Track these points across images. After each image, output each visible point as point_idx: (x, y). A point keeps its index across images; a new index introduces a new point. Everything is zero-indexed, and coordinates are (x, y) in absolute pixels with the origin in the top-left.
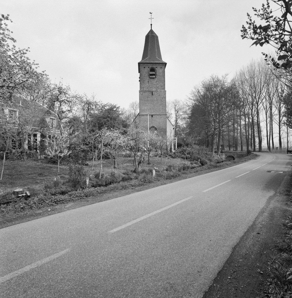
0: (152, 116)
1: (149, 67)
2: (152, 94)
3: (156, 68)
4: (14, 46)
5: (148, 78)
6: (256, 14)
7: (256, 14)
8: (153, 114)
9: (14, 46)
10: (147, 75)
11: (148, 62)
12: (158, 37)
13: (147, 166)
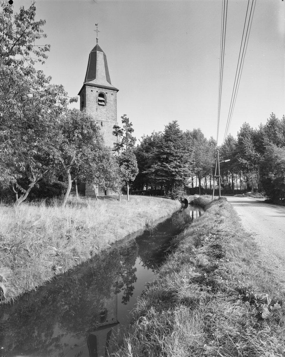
1: (97, 92)
2: (102, 124)
3: (106, 94)
5: (96, 105)
10: (95, 100)
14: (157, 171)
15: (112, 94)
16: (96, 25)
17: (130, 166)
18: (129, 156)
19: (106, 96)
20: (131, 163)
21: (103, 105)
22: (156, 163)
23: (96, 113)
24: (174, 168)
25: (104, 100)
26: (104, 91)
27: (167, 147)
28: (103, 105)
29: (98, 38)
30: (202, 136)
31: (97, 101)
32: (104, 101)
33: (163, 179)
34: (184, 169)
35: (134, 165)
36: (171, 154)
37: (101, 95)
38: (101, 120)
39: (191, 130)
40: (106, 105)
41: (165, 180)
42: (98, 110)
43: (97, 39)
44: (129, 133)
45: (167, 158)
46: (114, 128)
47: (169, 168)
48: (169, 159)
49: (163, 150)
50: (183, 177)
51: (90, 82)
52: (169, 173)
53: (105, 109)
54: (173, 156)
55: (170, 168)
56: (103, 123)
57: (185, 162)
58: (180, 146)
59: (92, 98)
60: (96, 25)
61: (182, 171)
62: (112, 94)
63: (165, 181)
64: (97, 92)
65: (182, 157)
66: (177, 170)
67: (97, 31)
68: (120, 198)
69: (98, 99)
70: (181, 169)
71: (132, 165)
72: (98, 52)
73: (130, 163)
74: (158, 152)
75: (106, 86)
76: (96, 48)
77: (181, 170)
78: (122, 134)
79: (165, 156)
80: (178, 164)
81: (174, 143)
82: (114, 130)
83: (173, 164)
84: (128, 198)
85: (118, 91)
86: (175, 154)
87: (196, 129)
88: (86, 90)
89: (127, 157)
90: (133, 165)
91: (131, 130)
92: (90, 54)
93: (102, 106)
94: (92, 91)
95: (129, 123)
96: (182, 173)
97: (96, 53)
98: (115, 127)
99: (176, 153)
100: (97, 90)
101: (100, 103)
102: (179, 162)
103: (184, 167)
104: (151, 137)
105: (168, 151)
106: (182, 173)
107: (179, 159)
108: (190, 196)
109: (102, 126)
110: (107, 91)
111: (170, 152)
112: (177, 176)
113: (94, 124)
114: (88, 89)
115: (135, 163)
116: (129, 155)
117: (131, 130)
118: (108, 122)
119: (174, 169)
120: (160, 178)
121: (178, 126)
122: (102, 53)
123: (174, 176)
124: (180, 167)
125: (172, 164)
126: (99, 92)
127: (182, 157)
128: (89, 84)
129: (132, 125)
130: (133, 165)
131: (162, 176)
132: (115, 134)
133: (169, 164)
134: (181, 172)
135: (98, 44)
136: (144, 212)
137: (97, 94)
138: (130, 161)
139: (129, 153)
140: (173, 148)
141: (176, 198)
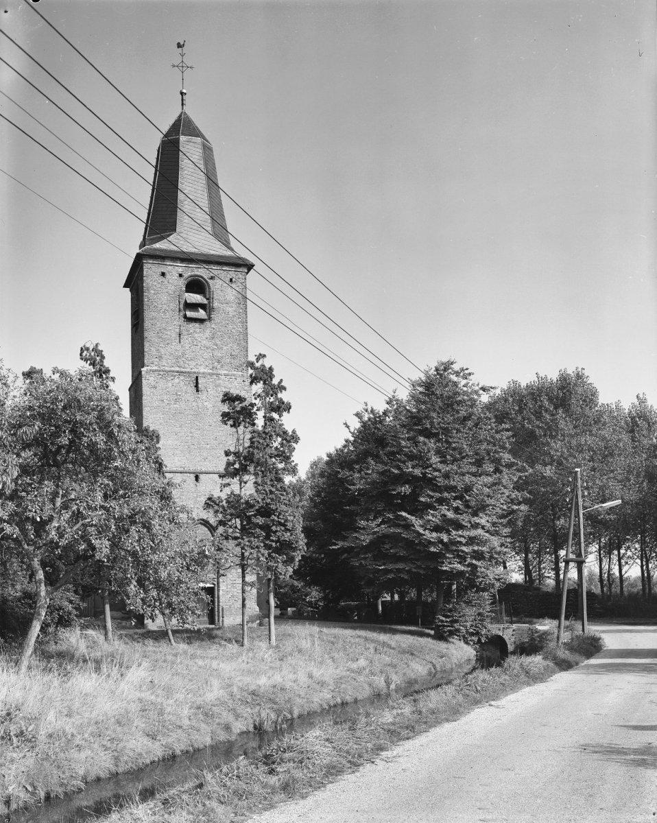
0: (197, 478)
1: (181, 275)
2: (197, 386)
3: (210, 282)
4: (54, 374)
5: (178, 321)
6: (467, 369)
7: (467, 369)
8: (199, 469)
9: (54, 374)
10: (174, 305)
11: (34, 6)
12: (212, 151)
13: (501, 427)
14: (379, 540)
15: (231, 280)
16: (179, 46)
17: (274, 528)
18: (273, 496)
19: (210, 288)
20: (276, 518)
21: (201, 321)
22: (378, 514)
23: (179, 347)
24: (437, 529)
25: (205, 301)
26: (202, 272)
27: (411, 457)
28: (201, 321)
29: (184, 91)
30: (590, 397)
31: (182, 306)
32: (203, 306)
33: (399, 571)
34: (473, 533)
35: (289, 525)
36: (430, 483)
37: (196, 285)
38: (196, 370)
39: (553, 376)
40: (210, 319)
41: (409, 572)
42: (184, 337)
43: (182, 93)
44: (275, 416)
45: (414, 496)
46: (223, 401)
47: (418, 533)
48: (422, 499)
49: (399, 468)
50: (469, 560)
51: (157, 245)
52: (417, 548)
53: (208, 333)
54: (437, 488)
55: (421, 531)
56: (200, 381)
57: (479, 509)
58: (461, 451)
59: (165, 298)
60: (179, 46)
61: (464, 541)
62: (231, 280)
63: (406, 577)
64: (181, 275)
65: (468, 489)
66: (445, 538)
67: (182, 67)
68: (246, 637)
69: (182, 302)
70: (460, 533)
71: (280, 524)
72: (182, 138)
73: (273, 520)
74: (382, 473)
75: (212, 252)
76: (183, 126)
77: (460, 536)
78: (254, 420)
79: (406, 489)
80: (450, 515)
81: (439, 440)
82: (226, 408)
83: (433, 517)
84: (273, 638)
85: (250, 267)
86: (441, 482)
87: (571, 371)
88: (145, 273)
89: (263, 499)
90: (284, 525)
91: (282, 407)
92: (159, 148)
93: (197, 325)
94: (163, 274)
95: (275, 381)
96: (464, 548)
97: (177, 142)
98: (228, 398)
99: (447, 476)
100: (180, 270)
101: (190, 314)
102: (457, 510)
103: (476, 526)
104: (385, 413)
105: (418, 472)
106: (464, 548)
107: (455, 498)
108: (514, 626)
109: (197, 391)
110: (216, 270)
111: (424, 474)
112: (447, 558)
113: (108, 417)
114: (151, 270)
115: (290, 518)
116: (271, 492)
117: (282, 407)
118: (218, 375)
119: (434, 535)
120: (390, 567)
121: (470, 374)
122: (199, 140)
123: (438, 557)
124: (459, 526)
125: (430, 518)
126: (186, 275)
127: (468, 489)
128: (152, 253)
129: (285, 389)
130: (284, 525)
131: (399, 559)
132: (231, 422)
133: (421, 518)
134: (460, 543)
135: (189, 110)
136: (275, 686)
137: (182, 284)
138: (273, 512)
139: (272, 486)
140: (435, 459)
141: (452, 633)
